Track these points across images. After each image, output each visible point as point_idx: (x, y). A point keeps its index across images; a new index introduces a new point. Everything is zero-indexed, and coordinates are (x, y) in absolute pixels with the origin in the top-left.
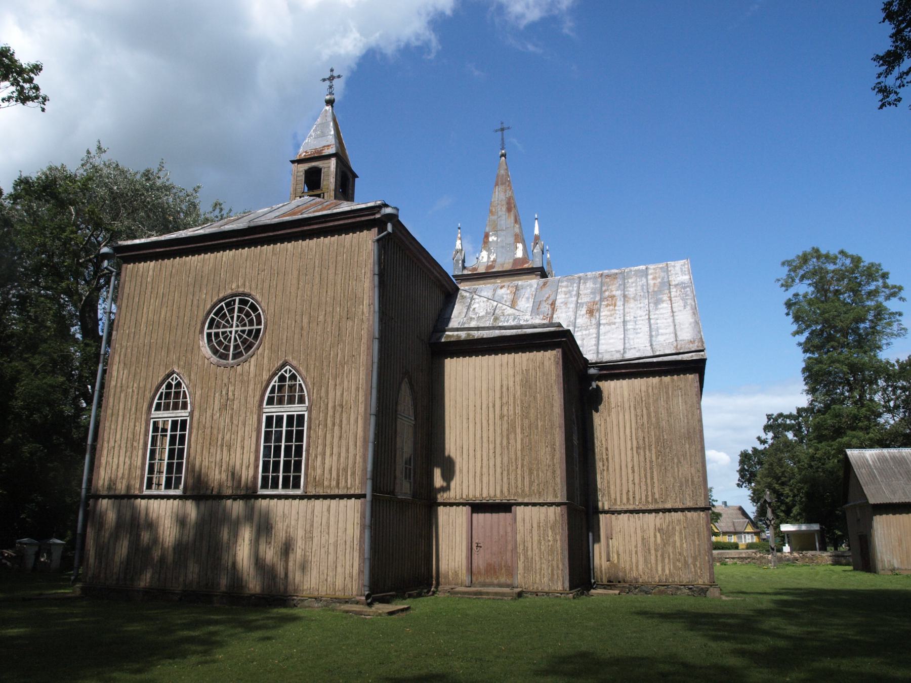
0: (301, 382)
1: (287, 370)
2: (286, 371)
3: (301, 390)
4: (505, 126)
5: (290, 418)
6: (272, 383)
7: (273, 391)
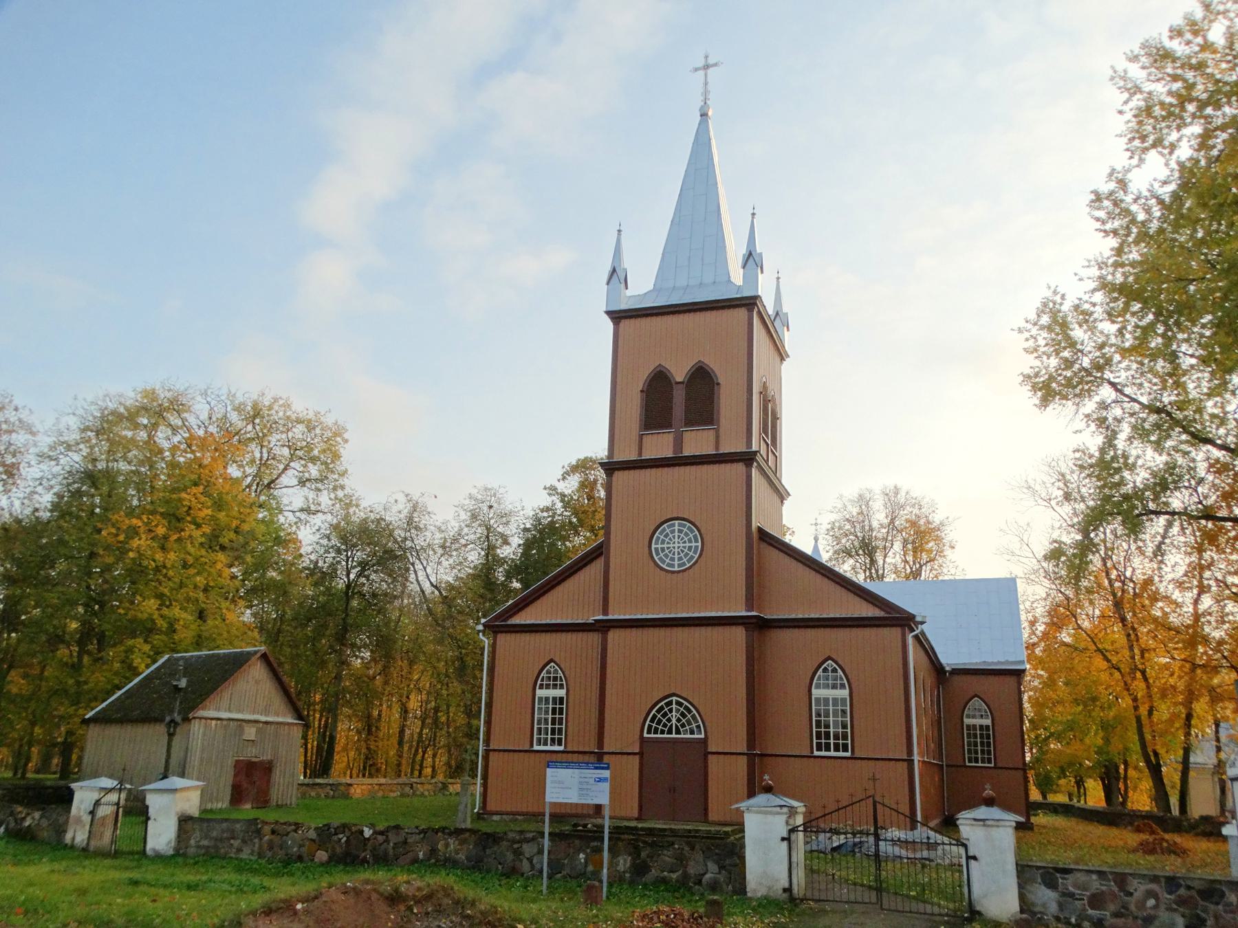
3: (561, 680)
4: (711, 61)
5: (555, 699)
7: (542, 680)
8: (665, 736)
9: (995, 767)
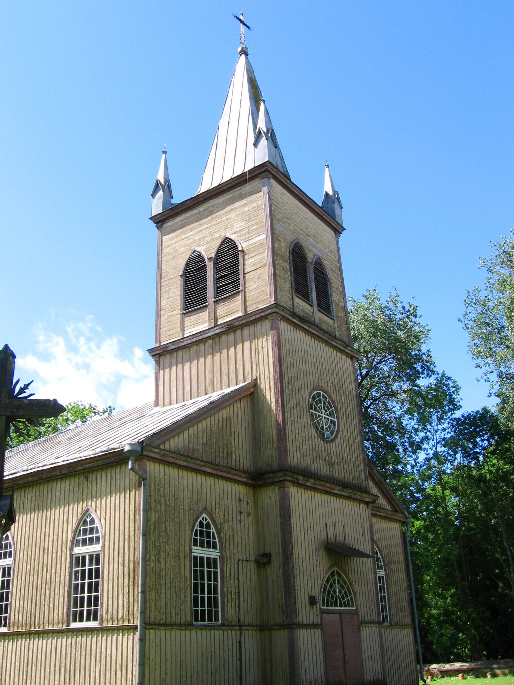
0: (214, 531)
1: (203, 517)
2: (203, 519)
6: (196, 528)
8: (339, 608)
9: (223, 625)
